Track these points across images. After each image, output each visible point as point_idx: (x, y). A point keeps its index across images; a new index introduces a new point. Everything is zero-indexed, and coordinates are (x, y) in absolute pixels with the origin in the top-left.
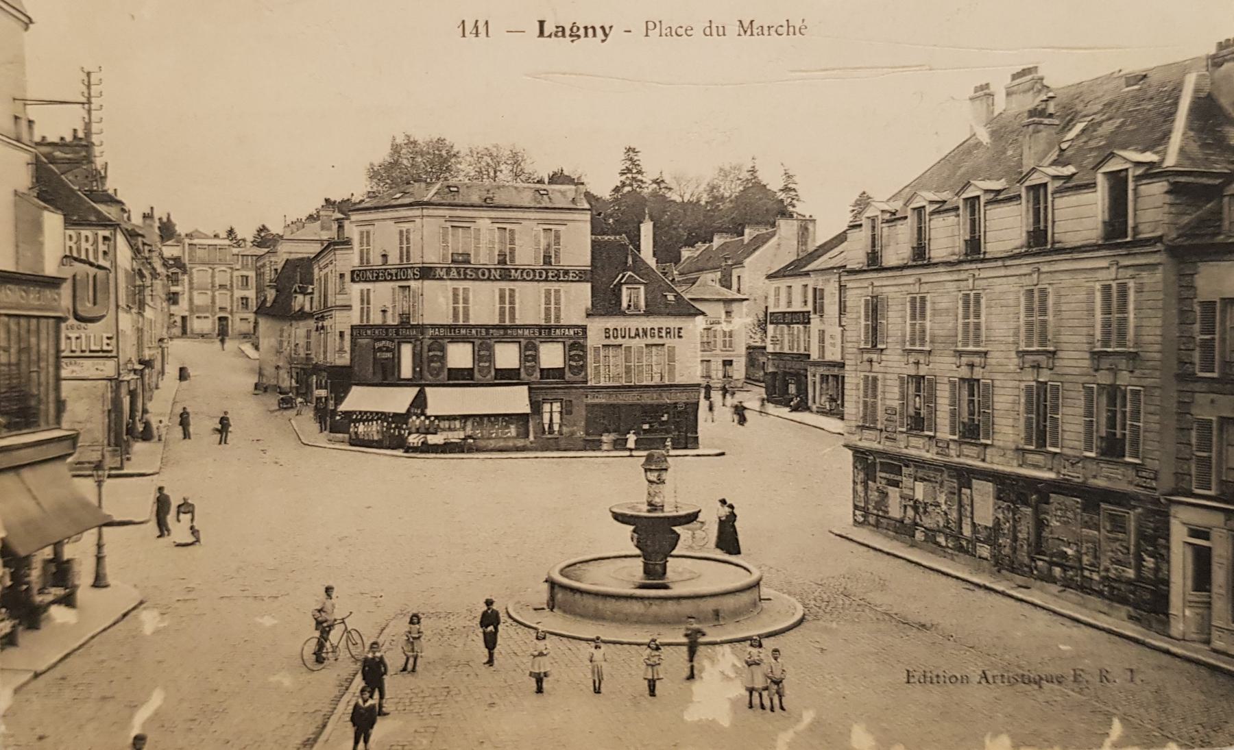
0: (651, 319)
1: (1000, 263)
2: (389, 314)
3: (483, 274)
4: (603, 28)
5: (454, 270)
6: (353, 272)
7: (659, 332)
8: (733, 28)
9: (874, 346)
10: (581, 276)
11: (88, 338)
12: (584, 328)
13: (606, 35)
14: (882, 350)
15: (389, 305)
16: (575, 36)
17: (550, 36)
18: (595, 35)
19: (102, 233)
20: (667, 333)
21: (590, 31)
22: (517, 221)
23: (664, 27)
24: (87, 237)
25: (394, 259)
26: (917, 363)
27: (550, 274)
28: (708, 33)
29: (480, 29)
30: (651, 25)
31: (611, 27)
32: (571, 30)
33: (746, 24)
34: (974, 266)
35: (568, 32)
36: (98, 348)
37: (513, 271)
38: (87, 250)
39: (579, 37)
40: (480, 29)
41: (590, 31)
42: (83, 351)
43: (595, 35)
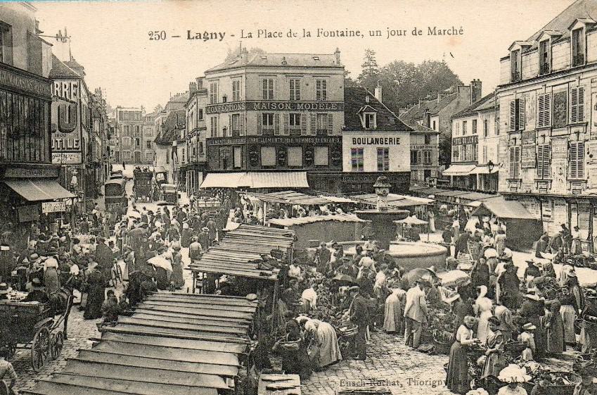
2: (228, 131)
3: (281, 107)
4: (220, 34)
6: (207, 107)
9: (517, 129)
10: (338, 107)
11: (66, 141)
12: (341, 138)
13: (222, 37)
14: (522, 131)
15: (228, 126)
17: (193, 38)
18: (216, 38)
19: (73, 83)
20: (390, 141)
21: (214, 36)
23: (267, 33)
24: (65, 86)
25: (230, 99)
28: (289, 35)
29: (161, 36)
30: (261, 32)
31: (224, 34)
32: (204, 35)
33: (432, 29)
36: (71, 147)
38: (65, 92)
39: (208, 38)
40: (161, 36)
41: (214, 36)
42: (58, 149)
43: (216, 38)
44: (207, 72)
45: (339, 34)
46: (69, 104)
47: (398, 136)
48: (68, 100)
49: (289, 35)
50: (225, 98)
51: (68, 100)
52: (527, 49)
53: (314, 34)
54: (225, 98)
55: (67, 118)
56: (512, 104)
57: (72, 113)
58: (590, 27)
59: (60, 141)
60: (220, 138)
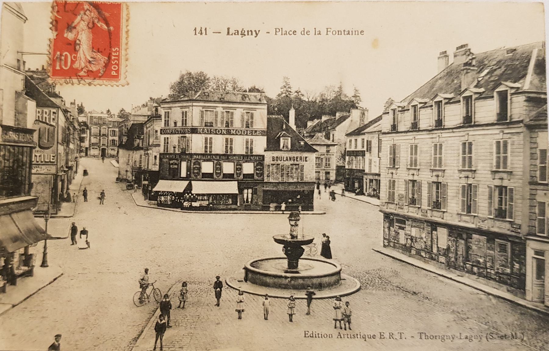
0: (294, 153)
1: (451, 131)
2: (177, 149)
4: (255, 31)
5: (206, 130)
7: (297, 159)
8: (312, 32)
11: (44, 156)
13: (257, 34)
16: (243, 35)
17: (232, 34)
18: (252, 34)
21: (250, 33)
22: (235, 109)
26: (438, 176)
27: (248, 132)
28: (303, 33)
31: (259, 31)
32: (242, 32)
34: (439, 132)
35: (240, 33)
36: (48, 161)
37: (232, 131)
38: (46, 118)
39: (245, 35)
41: (250, 33)
43: (252, 34)
44: (457, 49)
45: (346, 33)
46: (47, 127)
47: (306, 156)
48: (47, 124)
49: (303, 33)
50: (175, 123)
51: (47, 124)
52: (404, 110)
53: (324, 32)
54: (175, 123)
55: (47, 138)
56: (391, 147)
57: (51, 135)
58: (447, 101)
59: (39, 156)
60: (171, 154)
